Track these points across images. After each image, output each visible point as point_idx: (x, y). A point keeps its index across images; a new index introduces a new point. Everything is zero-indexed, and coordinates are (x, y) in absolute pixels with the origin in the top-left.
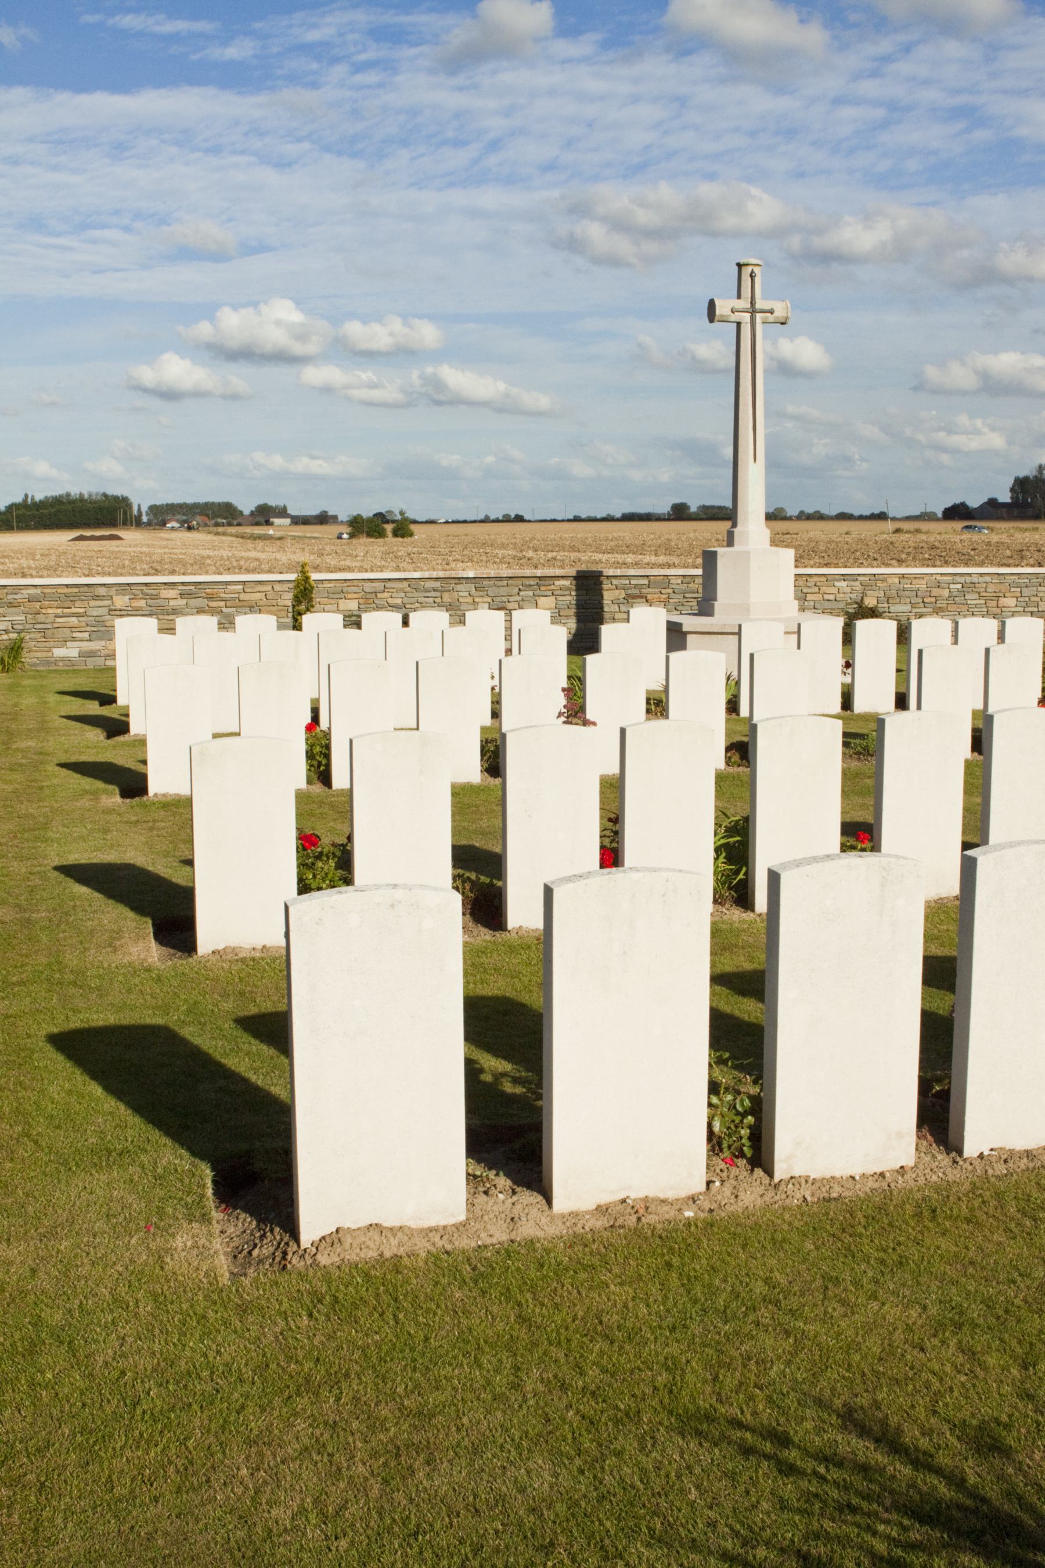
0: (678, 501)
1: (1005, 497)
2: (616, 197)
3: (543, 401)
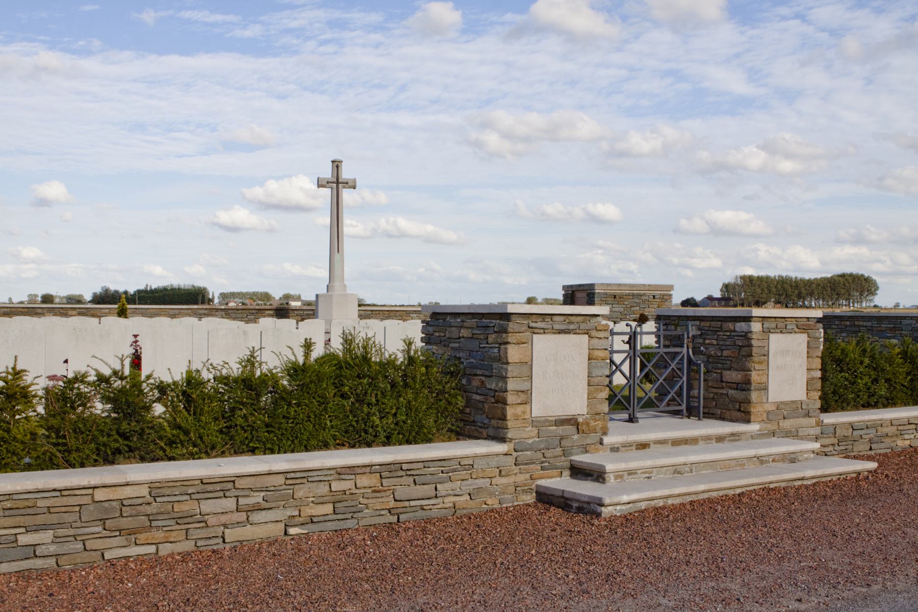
0: (530, 296)
1: (717, 294)
2: (503, 117)
3: (451, 236)
